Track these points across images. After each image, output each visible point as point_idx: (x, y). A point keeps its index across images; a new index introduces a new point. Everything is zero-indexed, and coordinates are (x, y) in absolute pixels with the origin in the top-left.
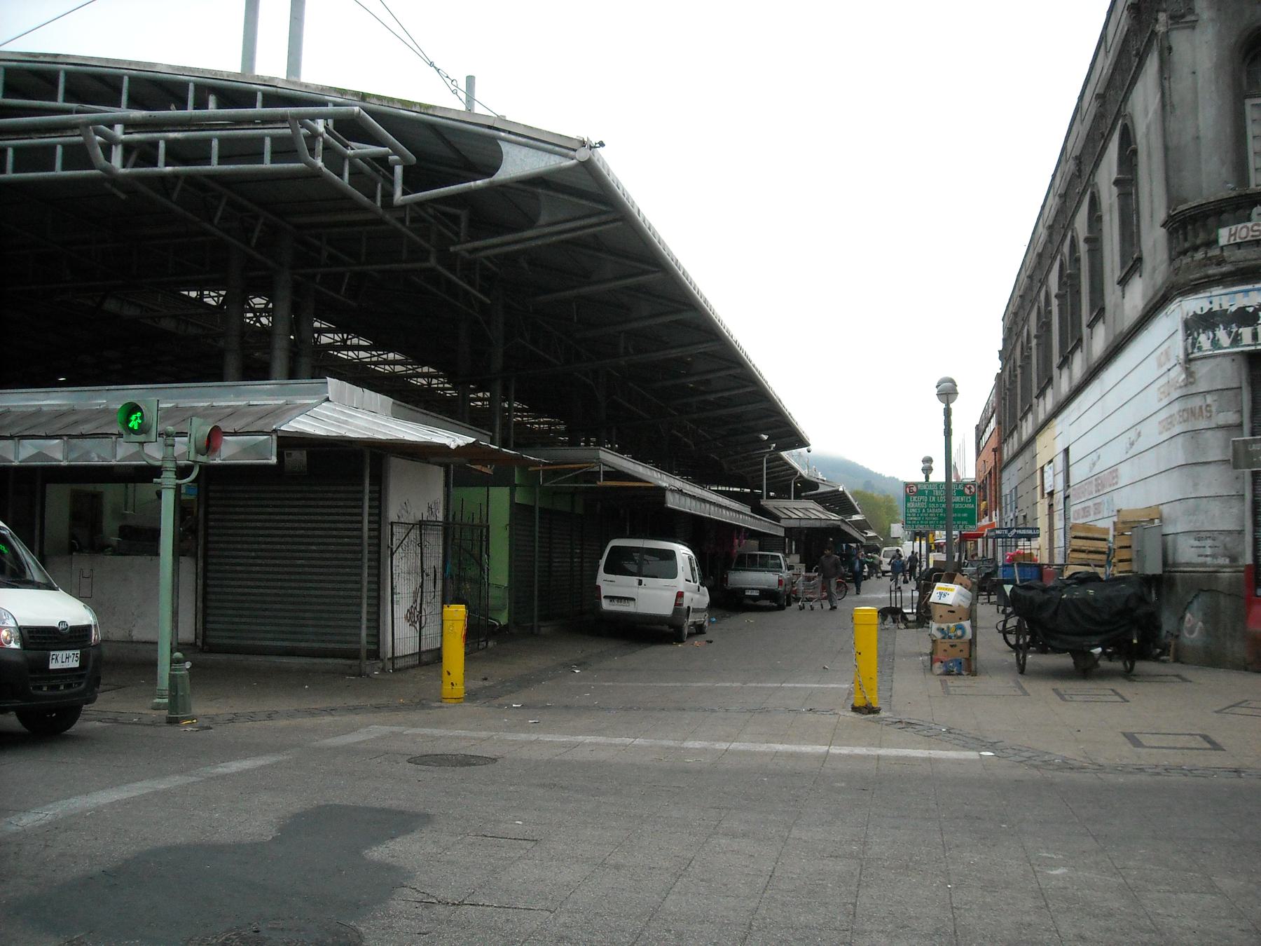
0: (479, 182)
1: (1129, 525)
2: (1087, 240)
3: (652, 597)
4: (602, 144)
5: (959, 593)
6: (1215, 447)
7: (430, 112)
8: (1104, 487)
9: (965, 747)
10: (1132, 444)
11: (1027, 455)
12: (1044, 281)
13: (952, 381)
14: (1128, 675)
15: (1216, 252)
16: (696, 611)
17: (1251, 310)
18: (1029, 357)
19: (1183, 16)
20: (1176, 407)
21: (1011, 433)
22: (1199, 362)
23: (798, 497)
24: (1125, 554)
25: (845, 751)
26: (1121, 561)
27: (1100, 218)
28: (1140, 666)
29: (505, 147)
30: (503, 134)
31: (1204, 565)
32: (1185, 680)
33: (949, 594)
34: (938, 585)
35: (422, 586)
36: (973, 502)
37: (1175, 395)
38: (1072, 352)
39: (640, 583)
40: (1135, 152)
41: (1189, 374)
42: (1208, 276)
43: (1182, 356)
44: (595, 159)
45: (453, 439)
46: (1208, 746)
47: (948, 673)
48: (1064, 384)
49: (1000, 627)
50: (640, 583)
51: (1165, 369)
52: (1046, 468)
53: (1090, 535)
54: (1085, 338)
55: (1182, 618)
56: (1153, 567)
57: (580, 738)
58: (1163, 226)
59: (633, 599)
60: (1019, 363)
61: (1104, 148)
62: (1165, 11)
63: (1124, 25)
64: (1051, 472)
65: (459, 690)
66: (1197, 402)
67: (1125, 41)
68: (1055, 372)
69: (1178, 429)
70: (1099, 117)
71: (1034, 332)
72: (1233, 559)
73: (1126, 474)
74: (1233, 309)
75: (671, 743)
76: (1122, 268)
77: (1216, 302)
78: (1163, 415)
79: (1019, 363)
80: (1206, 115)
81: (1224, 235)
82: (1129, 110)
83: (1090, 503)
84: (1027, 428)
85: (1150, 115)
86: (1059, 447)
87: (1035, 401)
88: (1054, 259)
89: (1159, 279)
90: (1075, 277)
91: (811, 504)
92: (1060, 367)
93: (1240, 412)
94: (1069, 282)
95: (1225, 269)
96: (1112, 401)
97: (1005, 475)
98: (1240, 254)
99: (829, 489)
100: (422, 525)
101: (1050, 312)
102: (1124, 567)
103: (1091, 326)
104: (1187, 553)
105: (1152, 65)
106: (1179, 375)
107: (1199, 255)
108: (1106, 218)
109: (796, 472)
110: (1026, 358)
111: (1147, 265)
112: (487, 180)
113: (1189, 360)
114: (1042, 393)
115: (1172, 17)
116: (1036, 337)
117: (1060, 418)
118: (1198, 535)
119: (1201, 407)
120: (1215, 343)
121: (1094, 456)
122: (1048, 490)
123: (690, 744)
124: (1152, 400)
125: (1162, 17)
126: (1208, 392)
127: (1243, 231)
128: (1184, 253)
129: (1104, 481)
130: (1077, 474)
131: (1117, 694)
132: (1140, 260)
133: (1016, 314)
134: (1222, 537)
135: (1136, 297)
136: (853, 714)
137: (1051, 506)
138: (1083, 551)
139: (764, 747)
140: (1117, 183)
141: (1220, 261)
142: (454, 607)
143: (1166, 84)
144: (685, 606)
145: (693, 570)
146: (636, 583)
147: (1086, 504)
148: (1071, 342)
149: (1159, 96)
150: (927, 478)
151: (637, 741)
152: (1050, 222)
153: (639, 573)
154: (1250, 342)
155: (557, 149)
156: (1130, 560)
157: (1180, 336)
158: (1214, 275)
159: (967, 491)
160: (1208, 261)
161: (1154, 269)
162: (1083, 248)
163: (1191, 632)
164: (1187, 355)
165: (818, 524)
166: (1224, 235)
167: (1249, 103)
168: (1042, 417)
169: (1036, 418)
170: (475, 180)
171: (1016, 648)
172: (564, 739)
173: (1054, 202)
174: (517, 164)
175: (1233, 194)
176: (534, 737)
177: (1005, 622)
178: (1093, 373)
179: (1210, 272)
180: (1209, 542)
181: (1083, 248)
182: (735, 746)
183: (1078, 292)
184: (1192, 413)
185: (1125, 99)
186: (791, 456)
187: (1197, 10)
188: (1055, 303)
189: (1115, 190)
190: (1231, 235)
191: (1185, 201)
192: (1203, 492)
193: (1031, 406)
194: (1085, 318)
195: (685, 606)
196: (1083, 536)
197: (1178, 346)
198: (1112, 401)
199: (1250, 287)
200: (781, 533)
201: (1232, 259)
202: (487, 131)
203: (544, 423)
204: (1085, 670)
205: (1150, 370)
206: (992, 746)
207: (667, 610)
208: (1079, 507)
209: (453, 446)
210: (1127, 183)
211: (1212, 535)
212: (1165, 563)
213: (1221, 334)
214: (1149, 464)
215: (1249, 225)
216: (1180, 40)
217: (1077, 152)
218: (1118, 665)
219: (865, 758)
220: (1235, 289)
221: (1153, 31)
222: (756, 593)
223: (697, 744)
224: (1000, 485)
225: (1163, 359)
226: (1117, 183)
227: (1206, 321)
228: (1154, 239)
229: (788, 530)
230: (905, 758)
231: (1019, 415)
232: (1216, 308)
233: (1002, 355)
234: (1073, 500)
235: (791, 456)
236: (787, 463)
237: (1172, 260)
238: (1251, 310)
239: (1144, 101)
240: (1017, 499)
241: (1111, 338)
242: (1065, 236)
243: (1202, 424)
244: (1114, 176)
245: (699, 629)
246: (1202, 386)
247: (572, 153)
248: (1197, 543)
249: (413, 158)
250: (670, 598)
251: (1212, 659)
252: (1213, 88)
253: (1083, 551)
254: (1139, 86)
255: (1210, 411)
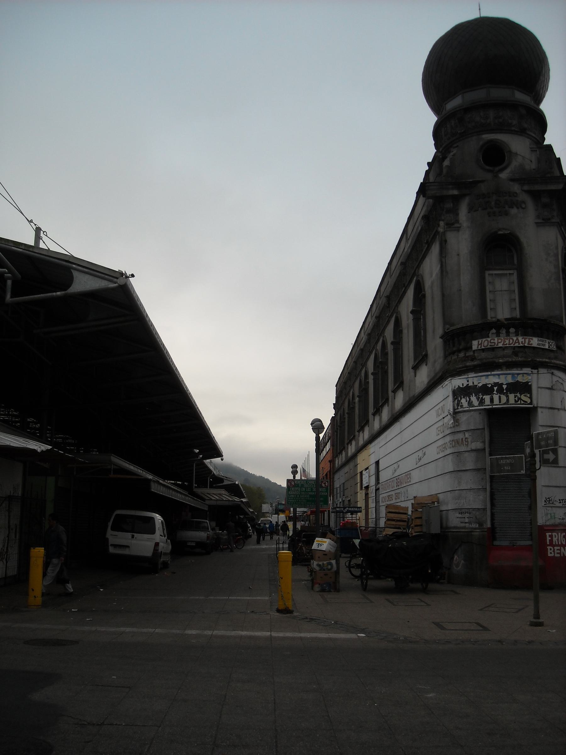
0: (59, 293)
1: (419, 504)
2: (392, 343)
3: (142, 545)
4: (133, 276)
5: (330, 544)
6: (470, 462)
7: (31, 249)
8: (401, 483)
9: (347, 631)
10: (420, 459)
11: (351, 465)
12: (364, 365)
13: (320, 421)
14: (425, 591)
15: (471, 353)
16: (165, 554)
17: (490, 386)
18: (354, 408)
19: (453, 224)
20: (448, 439)
21: (341, 452)
22: (461, 414)
23: (211, 487)
24: (418, 522)
25: (281, 635)
26: (416, 526)
27: (401, 332)
28: (431, 586)
29: (75, 274)
30: (74, 266)
31: (464, 528)
32: (456, 593)
33: (323, 544)
34: (317, 539)
35: (8, 537)
36: (327, 491)
37: (448, 432)
38: (382, 406)
39: (133, 537)
40: (424, 296)
41: (456, 421)
42: (466, 367)
43: (452, 410)
44: (128, 283)
45: (39, 447)
46: (481, 628)
47: (323, 590)
48: (376, 425)
49: (347, 564)
50: (133, 537)
51: (441, 417)
52: (364, 472)
53: (397, 511)
54: (390, 399)
55: (453, 558)
56: (435, 529)
57: (122, 629)
58: (441, 338)
59: (128, 547)
60: (346, 411)
61: (405, 293)
62: (443, 220)
63: (418, 227)
64: (367, 475)
65: (39, 600)
66: (460, 436)
67: (420, 235)
68: (371, 417)
69: (449, 451)
70: (402, 275)
71: (357, 393)
72: (481, 524)
73: (416, 476)
74: (480, 385)
75: (178, 632)
76: (415, 359)
77: (470, 380)
78: (440, 443)
79: (346, 411)
80: (465, 279)
81: (475, 344)
82: (421, 272)
83: (393, 493)
84: (352, 449)
85: (434, 276)
86: (373, 460)
87: (357, 433)
88: (371, 353)
89: (438, 366)
90: (385, 363)
91: (223, 492)
92: (374, 415)
93: (484, 442)
94: (381, 366)
95: (476, 363)
96: (407, 435)
97: (337, 477)
98: (483, 355)
99: (230, 483)
100: (10, 498)
101: (368, 382)
102: (418, 529)
103: (394, 391)
104: (454, 521)
105: (435, 249)
106: (449, 420)
107: (462, 355)
108: (405, 331)
109: (212, 471)
110: (351, 409)
111: (431, 358)
112: (63, 292)
113: (455, 413)
114: (362, 429)
115: (447, 224)
116: (358, 396)
117: (373, 444)
118: (461, 511)
119: (462, 439)
120: (470, 404)
121: (396, 466)
122: (365, 484)
123: (189, 632)
124: (433, 435)
125: (442, 223)
126: (466, 431)
127: (485, 343)
128: (453, 353)
129: (402, 481)
130: (384, 476)
131: (422, 601)
132: (426, 356)
133: (345, 383)
134: (474, 512)
135: (423, 377)
136: (278, 614)
137: (367, 494)
138: (394, 520)
139: (233, 633)
140: (412, 312)
141: (473, 359)
142: (38, 549)
143: (444, 260)
144: (160, 551)
145: (163, 529)
146: (130, 537)
147: (390, 493)
148: (382, 399)
149: (439, 266)
150: (294, 477)
151: (157, 630)
152: (369, 331)
153: (133, 531)
154: (498, 403)
155: (106, 276)
156: (421, 525)
157: (451, 398)
158: (470, 366)
159: (323, 485)
160: (466, 358)
161: (435, 362)
162: (390, 348)
163: (457, 566)
164: (454, 409)
165: (227, 503)
166: (475, 344)
167: (487, 273)
168: (361, 442)
169: (357, 443)
170: (56, 292)
171: (359, 577)
172: (113, 629)
173: (371, 321)
174: (82, 284)
175: (480, 322)
176: (94, 629)
177: (350, 561)
178: (395, 418)
179: (468, 364)
180: (467, 515)
181: (390, 348)
182: (215, 632)
183: (386, 372)
184: (457, 443)
185: (418, 267)
186: (213, 463)
187: (460, 221)
188: (371, 378)
189: (411, 316)
190: (478, 345)
191: (453, 325)
192: (464, 486)
193: (354, 436)
194: (391, 386)
195: (160, 551)
196: (394, 511)
197: (449, 404)
198: (407, 435)
199: (489, 373)
200: (206, 508)
201: (479, 358)
202: (64, 263)
203: (60, 438)
204: (401, 589)
205: (432, 418)
206: (362, 631)
207: (148, 553)
208: (385, 495)
209: (39, 450)
210: (419, 311)
211: (469, 511)
212: (442, 527)
213: (474, 399)
214: (431, 471)
215: (489, 339)
216: (451, 237)
217: (387, 293)
218: (418, 585)
219: (293, 639)
220: (480, 374)
221: (437, 231)
222: (194, 544)
223: (194, 632)
224: (333, 482)
225: (440, 411)
226: (412, 312)
227: (458, 393)
228: (435, 344)
229: (210, 506)
230: (316, 638)
231: (346, 441)
232: (471, 384)
233: (335, 406)
234: (381, 491)
235: (213, 463)
236: (207, 467)
237: (446, 357)
238: (490, 386)
239: (430, 268)
240: (344, 490)
241: (407, 399)
242: (378, 340)
243: (463, 449)
244: (411, 308)
245: (165, 565)
246: (463, 428)
247: (115, 280)
248: (460, 516)
249: (19, 276)
250: (152, 545)
251: (470, 581)
252: (469, 264)
253: (394, 520)
254: (427, 260)
255: (468, 442)
